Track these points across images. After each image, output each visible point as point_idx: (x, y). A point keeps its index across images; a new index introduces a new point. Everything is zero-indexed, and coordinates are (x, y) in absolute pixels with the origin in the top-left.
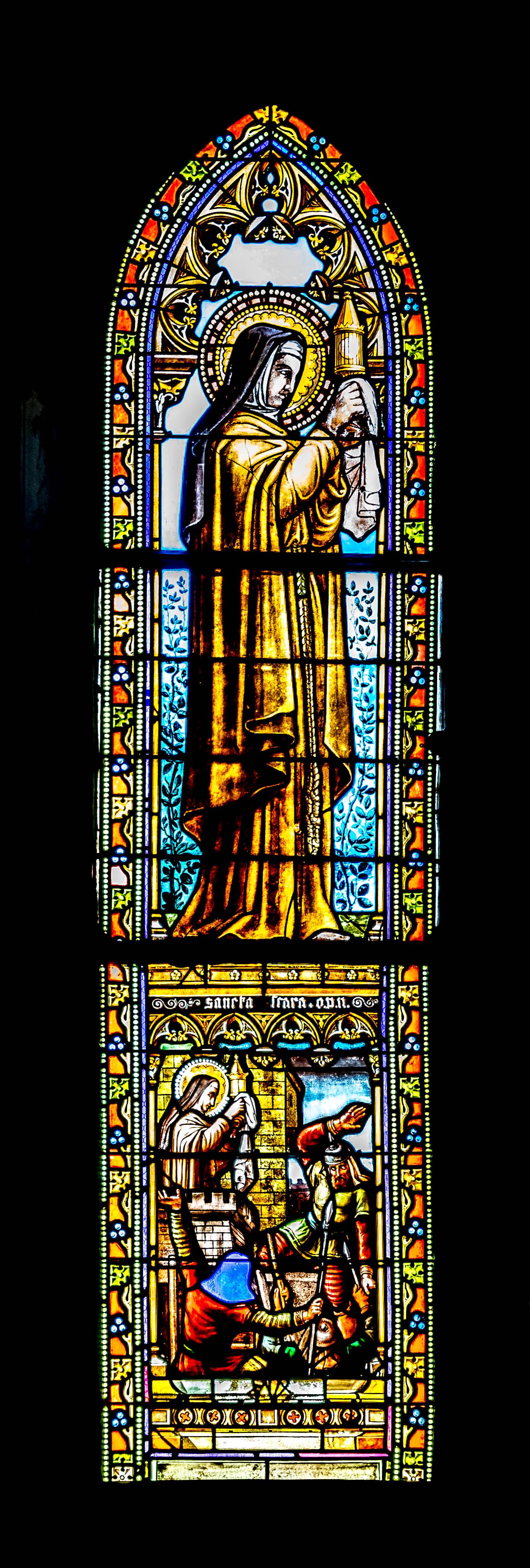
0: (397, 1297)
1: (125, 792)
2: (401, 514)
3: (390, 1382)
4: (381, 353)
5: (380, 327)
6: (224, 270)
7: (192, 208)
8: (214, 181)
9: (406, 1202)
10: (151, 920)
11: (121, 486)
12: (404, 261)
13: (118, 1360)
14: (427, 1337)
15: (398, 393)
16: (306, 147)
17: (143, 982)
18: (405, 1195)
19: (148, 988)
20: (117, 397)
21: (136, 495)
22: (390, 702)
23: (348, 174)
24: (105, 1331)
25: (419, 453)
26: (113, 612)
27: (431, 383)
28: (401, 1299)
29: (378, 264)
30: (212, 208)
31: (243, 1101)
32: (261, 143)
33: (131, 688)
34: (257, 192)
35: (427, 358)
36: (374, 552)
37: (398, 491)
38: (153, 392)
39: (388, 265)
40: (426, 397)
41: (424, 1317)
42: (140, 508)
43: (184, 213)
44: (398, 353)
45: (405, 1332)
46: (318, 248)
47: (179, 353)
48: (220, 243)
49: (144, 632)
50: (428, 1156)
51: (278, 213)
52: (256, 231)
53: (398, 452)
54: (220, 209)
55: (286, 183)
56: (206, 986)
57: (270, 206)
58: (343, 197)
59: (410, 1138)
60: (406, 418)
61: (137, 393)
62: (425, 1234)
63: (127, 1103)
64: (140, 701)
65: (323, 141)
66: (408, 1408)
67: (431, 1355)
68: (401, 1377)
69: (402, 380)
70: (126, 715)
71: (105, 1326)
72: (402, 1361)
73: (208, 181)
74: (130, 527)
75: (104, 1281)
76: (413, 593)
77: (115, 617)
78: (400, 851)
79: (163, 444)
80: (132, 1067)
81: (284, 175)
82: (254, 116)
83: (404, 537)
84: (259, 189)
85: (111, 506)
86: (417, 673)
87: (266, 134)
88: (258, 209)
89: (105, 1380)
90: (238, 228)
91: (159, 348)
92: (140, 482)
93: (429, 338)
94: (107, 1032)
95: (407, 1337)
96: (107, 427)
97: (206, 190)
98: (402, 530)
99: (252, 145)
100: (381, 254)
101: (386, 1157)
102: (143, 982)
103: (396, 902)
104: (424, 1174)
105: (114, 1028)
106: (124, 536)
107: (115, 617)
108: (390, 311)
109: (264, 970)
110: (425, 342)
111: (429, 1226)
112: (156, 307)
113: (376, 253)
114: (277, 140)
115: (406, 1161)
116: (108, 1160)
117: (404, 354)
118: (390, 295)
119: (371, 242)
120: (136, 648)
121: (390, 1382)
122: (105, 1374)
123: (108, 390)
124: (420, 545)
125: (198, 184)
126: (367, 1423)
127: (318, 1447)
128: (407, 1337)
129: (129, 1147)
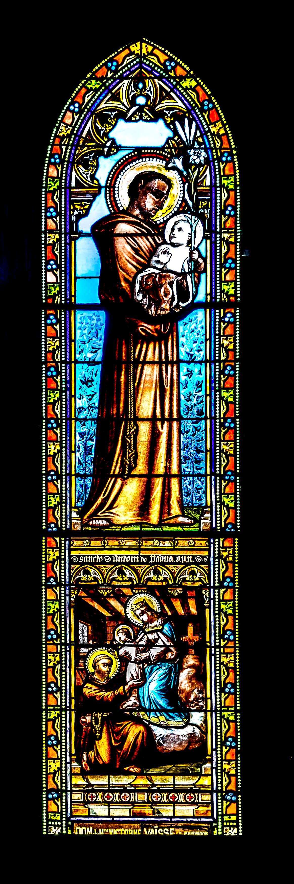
1: (55, 281)
4: (208, 184)
6: (113, 140)
9: (226, 781)
11: (51, 320)
12: (222, 132)
14: (237, 805)
15: (218, 207)
17: (67, 546)
18: (225, 776)
19: (70, 550)
21: (62, 799)
25: (230, 614)
26: (47, 600)
29: (206, 132)
30: (105, 103)
32: (134, 65)
33: (58, 380)
36: (204, 301)
39: (213, 134)
48: (109, 124)
50: (237, 590)
51: (146, 104)
52: (133, 115)
54: (111, 104)
55: (150, 88)
57: (141, 101)
59: (226, 636)
62: (236, 266)
63: (58, 405)
66: (224, 364)
67: (237, 602)
69: (221, 200)
78: (220, 471)
79: (78, 242)
82: (130, 50)
83: (222, 291)
87: (138, 60)
88: (133, 103)
90: (122, 115)
91: (73, 184)
94: (46, 681)
99: (129, 66)
100: (208, 127)
101: (213, 649)
102: (67, 546)
103: (218, 288)
108: (214, 160)
111: (238, 262)
114: (145, 64)
115: (224, 650)
116: (46, 647)
117: (222, 186)
118: (214, 151)
120: (61, 357)
126: (200, 801)
129: (59, 640)
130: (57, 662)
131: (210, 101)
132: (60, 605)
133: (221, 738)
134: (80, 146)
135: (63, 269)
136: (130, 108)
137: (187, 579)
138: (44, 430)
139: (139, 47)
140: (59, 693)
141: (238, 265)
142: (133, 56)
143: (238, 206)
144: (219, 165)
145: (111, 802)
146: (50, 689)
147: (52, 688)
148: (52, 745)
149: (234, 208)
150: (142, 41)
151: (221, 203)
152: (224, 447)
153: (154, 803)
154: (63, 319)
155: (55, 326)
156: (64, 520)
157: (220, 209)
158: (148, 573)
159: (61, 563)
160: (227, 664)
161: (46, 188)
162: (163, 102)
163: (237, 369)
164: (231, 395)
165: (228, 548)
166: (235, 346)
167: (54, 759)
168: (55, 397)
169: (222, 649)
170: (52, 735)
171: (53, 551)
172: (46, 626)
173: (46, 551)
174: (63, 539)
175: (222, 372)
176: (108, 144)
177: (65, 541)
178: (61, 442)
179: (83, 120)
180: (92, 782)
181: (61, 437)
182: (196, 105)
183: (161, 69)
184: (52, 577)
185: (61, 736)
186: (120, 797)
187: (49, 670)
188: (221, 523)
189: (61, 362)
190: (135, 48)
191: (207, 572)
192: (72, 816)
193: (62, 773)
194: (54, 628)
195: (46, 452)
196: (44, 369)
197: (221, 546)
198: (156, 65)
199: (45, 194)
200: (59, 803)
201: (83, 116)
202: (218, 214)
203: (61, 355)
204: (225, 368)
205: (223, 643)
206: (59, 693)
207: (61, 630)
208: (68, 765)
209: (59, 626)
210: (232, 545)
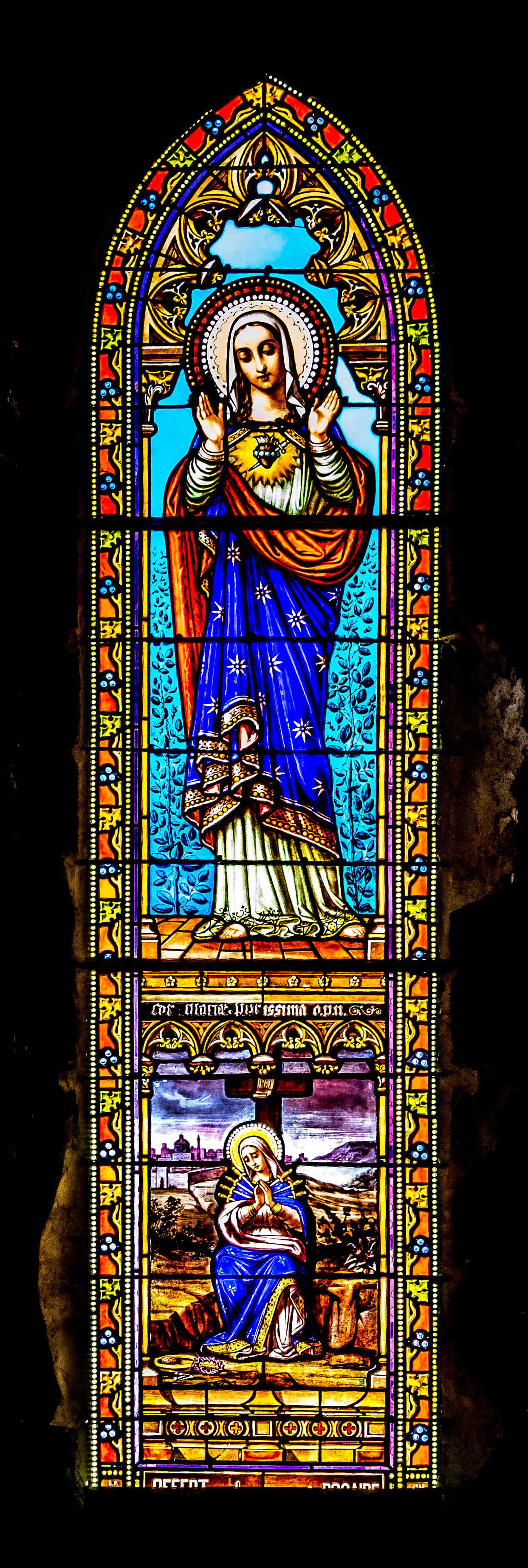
0: (400, 1455)
1: (114, 896)
5: (383, 309)
6: (217, 258)
10: (141, 925)
12: (407, 244)
13: (108, 1373)
16: (302, 128)
20: (103, 1341)
24: (95, 1437)
30: (201, 195)
31: (237, 884)
35: (430, 826)
37: (401, 586)
41: (428, 1242)
44: (400, 724)
46: (315, 229)
47: (168, 344)
48: (210, 230)
52: (250, 214)
57: (265, 188)
61: (124, 1337)
63: (118, 833)
66: (411, 1425)
67: (435, 712)
68: (403, 1019)
69: (403, 1040)
71: (94, 1339)
74: (118, 910)
75: (94, 1201)
77: (102, 622)
78: (403, 953)
80: (124, 891)
85: (97, 986)
86: (420, 1430)
87: (258, 117)
88: (252, 193)
90: (231, 214)
91: (144, 912)
95: (408, 880)
96: (93, 1070)
98: (404, 1007)
104: (429, 810)
105: (105, 466)
106: (111, 919)
122: (94, 1387)
125: (186, 170)
126: (366, 1435)
128: (408, 880)
130: (118, 437)
133: (405, 578)
134: (158, 269)
139: (259, 94)
141: (434, 774)
142: (249, 109)
143: (437, 378)
144: (401, 303)
145: (211, 1437)
146: (103, 778)
147: (108, 681)
148: (108, 596)
149: (430, 581)
150: (266, 81)
151: (403, 1045)
152: (411, 1382)
153: (285, 1440)
155: (113, 692)
156: (128, 985)
159: (124, 1115)
161: (98, 344)
162: (303, 190)
166: (433, 436)
167: (110, 1278)
168: (113, 726)
169: (410, 409)
170: (107, 474)
171: (110, 1002)
174: (128, 974)
175: (406, 774)
176: (209, 266)
177: (131, 977)
178: (124, 620)
180: (179, 1401)
181: (124, 798)
182: (361, 197)
183: (300, 132)
184: (109, 1048)
187: (102, 1119)
188: (404, 1236)
190: (254, 95)
191: (384, 1035)
192: (141, 1461)
193: (124, 1021)
197: (406, 800)
198: (289, 124)
199: (97, 556)
202: (399, 1064)
205: (411, 399)
207: (124, 1332)
208: (136, 1374)
210: (426, 706)
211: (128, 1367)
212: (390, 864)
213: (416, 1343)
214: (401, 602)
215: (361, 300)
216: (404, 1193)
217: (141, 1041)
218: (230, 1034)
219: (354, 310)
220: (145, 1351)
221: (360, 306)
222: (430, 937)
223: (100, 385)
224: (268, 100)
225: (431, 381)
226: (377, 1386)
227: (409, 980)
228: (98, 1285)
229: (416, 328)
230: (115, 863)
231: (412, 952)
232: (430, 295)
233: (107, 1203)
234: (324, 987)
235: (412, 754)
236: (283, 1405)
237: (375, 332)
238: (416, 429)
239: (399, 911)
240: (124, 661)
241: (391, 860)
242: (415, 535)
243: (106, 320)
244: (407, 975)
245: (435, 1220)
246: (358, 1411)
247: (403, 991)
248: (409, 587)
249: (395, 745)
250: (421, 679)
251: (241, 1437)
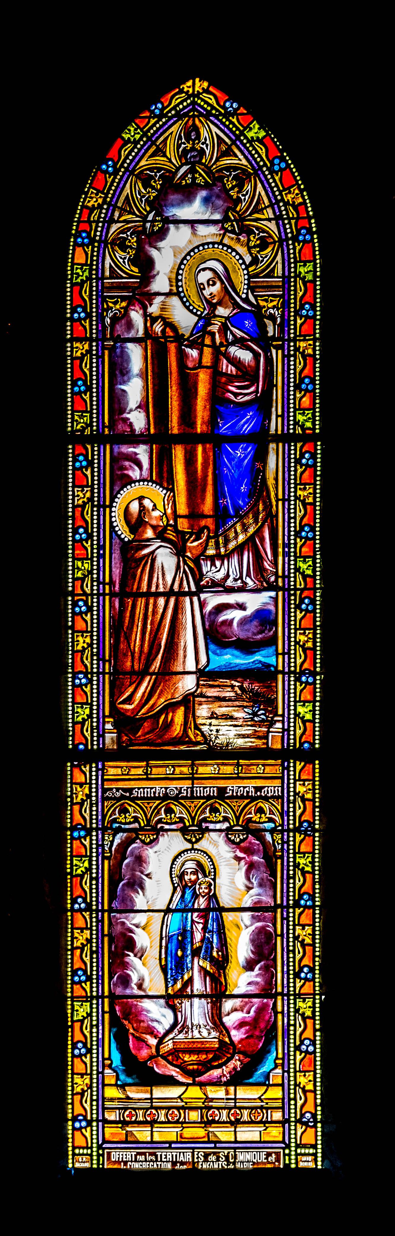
2: (295, 697)
3: (286, 656)
4: (280, 273)
5: (280, 253)
7: (132, 161)
8: (149, 139)
9: (301, 1099)
10: (104, 723)
20: (76, 979)
22: (286, 550)
23: (255, 131)
27: (318, 374)
28: (295, 513)
34: (183, 146)
38: (104, 310)
39: (286, 204)
40: (315, 605)
42: (95, 625)
43: (126, 165)
45: (298, 1053)
49: (97, 1016)
53: (292, 353)
55: (206, 139)
56: (148, 779)
58: (251, 149)
60: (297, 917)
61: (92, 606)
62: (315, 609)
64: (95, 555)
65: (235, 105)
67: (318, 686)
70: (84, 495)
72: (295, 706)
73: (145, 139)
76: (301, 906)
77: (75, 1076)
78: (295, 743)
81: (204, 133)
83: (296, 423)
84: (184, 143)
87: (189, 101)
89: (70, 576)
91: (107, 273)
92: (95, 530)
93: (317, 856)
97: (142, 146)
98: (295, 710)
100: (280, 194)
104: (314, 930)
107: (75, 1076)
109: (192, 766)
110: (315, 489)
111: (318, 309)
112: (104, 242)
113: (277, 193)
117: (298, 275)
119: (273, 185)
121: (286, 656)
123: (69, 311)
124: (309, 429)
127: (233, 1140)
130: (86, 868)
131: (283, 159)
132: (91, 710)
133: (295, 454)
135: (94, 352)
136: (180, 167)
137: (254, 819)
138: (70, 472)
140: (88, 1056)
141: (318, 607)
149: (313, 307)
154: (94, 386)
155: (83, 1058)
157: (295, 382)
158: (203, 812)
160: (304, 644)
163: (317, 382)
164: (309, 418)
165: (306, 784)
167: (82, 1075)
168: (84, 642)
172: (72, 1036)
173: (73, 491)
179: (118, 183)
180: (131, 1095)
185: (91, 897)
186: (166, 1115)
187: (75, 1097)
188: (294, 966)
189: (92, 595)
194: (84, 452)
195: (73, 646)
196: (69, 383)
200: (88, 1134)
201: (119, 177)
203: (91, 363)
204: (302, 601)
206: (88, 983)
209: (89, 738)
211: (95, 1072)
212: (285, 995)
213: (302, 902)
214: (292, 1032)
215: (263, 245)
216: (295, 787)
217: (104, 816)
218: (169, 811)
219: (258, 252)
220: (107, 713)
221: (263, 249)
222: (314, 731)
223: (74, 384)
224: (197, 89)
225: (313, 307)
226: (275, 1082)
227: (299, 767)
228: (72, 347)
229: (303, 414)
230: (84, 828)
231: (301, 744)
232: (316, 241)
233: (80, 719)
234: (238, 774)
235: (302, 591)
236: (207, 1098)
237: (273, 270)
238: (302, 270)
239: (292, 567)
240: (91, 296)
241: (286, 670)
242: (301, 420)
243: (79, 699)
244: (298, 763)
245: (317, 810)
246: (262, 1102)
247: (295, 775)
248: (297, 975)
249: (289, 667)
250: (308, 605)
251: (177, 1122)
